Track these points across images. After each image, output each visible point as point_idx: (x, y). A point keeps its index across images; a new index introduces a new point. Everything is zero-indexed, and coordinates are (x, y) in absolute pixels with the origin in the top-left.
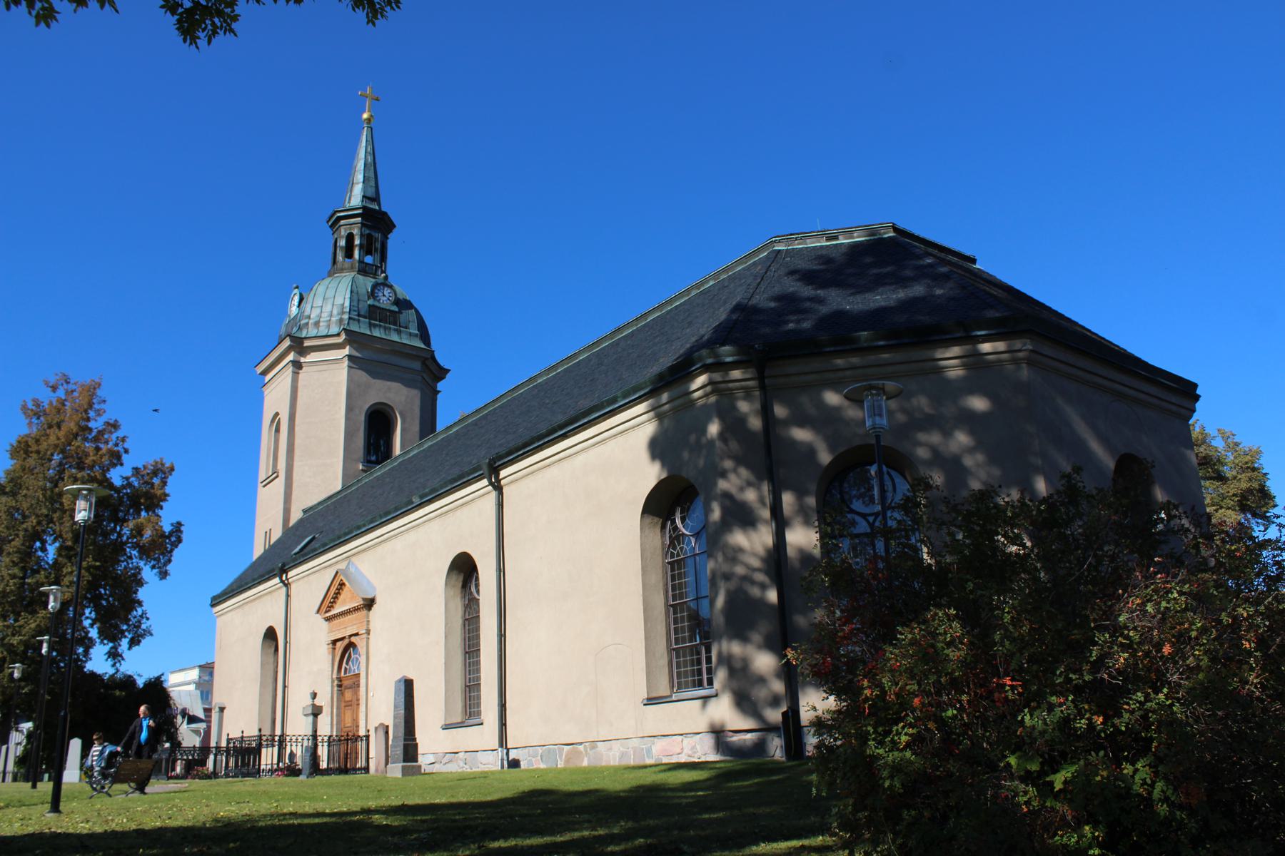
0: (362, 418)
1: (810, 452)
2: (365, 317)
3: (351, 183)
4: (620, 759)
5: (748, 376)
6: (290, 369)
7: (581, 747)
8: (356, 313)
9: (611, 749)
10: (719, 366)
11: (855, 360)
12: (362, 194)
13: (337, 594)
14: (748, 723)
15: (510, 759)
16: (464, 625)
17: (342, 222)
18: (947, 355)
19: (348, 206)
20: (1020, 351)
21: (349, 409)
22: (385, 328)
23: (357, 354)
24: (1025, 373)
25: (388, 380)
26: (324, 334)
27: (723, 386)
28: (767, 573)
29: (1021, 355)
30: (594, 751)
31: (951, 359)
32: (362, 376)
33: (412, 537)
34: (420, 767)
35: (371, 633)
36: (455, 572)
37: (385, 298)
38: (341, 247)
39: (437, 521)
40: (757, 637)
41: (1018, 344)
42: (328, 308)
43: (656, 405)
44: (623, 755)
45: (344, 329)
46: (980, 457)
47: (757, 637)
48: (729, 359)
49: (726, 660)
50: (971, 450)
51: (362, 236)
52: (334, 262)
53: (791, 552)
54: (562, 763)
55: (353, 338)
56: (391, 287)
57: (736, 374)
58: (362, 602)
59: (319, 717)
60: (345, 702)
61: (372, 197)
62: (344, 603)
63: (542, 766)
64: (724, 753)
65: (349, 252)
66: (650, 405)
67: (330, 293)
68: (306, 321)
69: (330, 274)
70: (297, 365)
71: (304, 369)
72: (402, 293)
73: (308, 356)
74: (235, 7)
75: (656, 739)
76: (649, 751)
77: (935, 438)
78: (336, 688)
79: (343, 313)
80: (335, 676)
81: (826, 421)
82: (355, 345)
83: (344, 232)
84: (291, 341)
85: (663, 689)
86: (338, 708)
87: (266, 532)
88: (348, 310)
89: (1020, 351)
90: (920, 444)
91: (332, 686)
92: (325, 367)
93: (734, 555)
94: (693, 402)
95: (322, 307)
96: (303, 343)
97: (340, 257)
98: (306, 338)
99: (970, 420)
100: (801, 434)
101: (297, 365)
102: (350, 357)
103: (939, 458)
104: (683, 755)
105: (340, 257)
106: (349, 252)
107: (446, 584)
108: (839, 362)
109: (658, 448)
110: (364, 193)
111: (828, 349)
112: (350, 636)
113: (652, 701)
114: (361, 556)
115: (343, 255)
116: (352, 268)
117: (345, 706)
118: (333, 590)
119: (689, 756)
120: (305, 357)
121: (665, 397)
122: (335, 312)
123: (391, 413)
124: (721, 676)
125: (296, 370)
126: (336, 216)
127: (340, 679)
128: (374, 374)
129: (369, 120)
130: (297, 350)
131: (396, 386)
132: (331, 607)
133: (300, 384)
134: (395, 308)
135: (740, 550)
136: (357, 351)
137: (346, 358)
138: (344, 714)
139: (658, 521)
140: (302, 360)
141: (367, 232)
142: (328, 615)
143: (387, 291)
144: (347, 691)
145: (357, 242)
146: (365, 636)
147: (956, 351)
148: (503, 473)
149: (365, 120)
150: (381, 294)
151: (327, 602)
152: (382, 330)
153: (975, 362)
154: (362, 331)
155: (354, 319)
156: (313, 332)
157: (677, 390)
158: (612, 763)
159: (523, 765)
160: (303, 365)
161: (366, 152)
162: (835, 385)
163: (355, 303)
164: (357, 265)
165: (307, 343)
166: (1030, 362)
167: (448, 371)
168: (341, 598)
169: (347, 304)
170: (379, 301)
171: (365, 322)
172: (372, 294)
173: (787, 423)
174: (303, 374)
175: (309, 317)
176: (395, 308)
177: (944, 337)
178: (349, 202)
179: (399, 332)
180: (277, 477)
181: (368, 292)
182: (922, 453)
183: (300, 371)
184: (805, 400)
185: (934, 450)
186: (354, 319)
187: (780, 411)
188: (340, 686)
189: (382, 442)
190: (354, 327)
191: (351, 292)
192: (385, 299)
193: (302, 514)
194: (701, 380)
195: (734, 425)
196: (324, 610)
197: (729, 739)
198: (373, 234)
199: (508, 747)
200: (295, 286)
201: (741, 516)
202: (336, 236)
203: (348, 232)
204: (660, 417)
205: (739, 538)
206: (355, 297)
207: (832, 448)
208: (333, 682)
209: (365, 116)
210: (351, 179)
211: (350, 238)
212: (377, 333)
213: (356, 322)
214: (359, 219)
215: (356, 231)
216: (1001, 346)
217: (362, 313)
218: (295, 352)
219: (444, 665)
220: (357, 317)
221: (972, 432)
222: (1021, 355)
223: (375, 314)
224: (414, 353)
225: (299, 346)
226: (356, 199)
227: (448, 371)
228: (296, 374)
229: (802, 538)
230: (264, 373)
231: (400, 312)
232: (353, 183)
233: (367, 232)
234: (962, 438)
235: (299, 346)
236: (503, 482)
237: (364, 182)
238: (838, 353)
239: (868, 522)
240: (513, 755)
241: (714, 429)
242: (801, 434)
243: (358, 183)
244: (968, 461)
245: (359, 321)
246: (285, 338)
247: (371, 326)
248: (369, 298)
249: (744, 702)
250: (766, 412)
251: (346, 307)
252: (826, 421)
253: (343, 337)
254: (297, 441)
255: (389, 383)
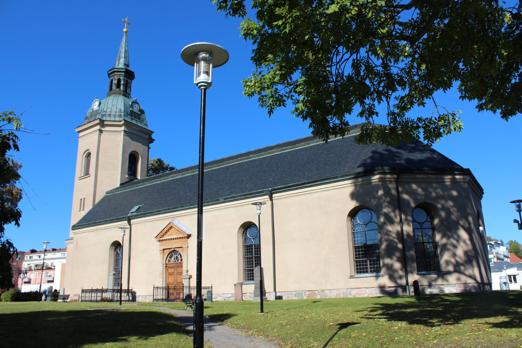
0: (128, 156)
1: (408, 202)
2: (129, 115)
3: (118, 57)
4: (336, 296)
5: (391, 177)
6: (98, 132)
7: (316, 292)
8: (126, 113)
9: (331, 292)
10: (384, 173)
11: (422, 176)
12: (124, 63)
13: (166, 233)
14: (392, 284)
15: (277, 296)
16: (243, 247)
17: (116, 73)
18: (447, 178)
19: (118, 67)
20: (466, 179)
21: (124, 152)
22: (136, 121)
23: (126, 130)
24: (466, 185)
25: (137, 142)
26: (109, 120)
27: (384, 179)
28: (397, 239)
29: (466, 180)
30: (323, 293)
31: (448, 179)
32: (128, 139)
33: (216, 213)
34: (267, 298)
35: (189, 247)
36: (242, 228)
37: (136, 108)
38: (115, 84)
39: (232, 208)
40: (395, 258)
41: (465, 177)
42: (114, 109)
43: (356, 182)
44: (337, 294)
45: (124, 119)
46: (455, 209)
47: (395, 258)
48: (388, 171)
49: (385, 265)
50: (452, 207)
51: (124, 80)
52: (111, 89)
53: (405, 233)
54: (306, 297)
55: (127, 124)
56: (138, 104)
57: (388, 176)
58: (187, 236)
59: (191, 279)
60: (169, 273)
61: (127, 65)
62: (172, 235)
63: (295, 298)
64: (383, 294)
65: (118, 85)
66: (353, 181)
67: (115, 103)
68: (105, 113)
69: (109, 95)
70: (101, 131)
71: (103, 133)
72: (142, 108)
73: (105, 128)
74: (438, 90)
75: (353, 289)
76: (350, 294)
77: (443, 202)
78: (165, 268)
79: (121, 112)
80: (164, 263)
81: (413, 193)
82: (126, 126)
83: (116, 78)
84: (100, 121)
85: (353, 274)
86: (166, 275)
87: (81, 199)
88: (123, 111)
89: (466, 179)
90: (439, 203)
91: (163, 267)
92: (112, 134)
93: (388, 233)
94: (371, 183)
95: (111, 108)
96: (104, 122)
97: (114, 87)
98: (105, 121)
99: (452, 198)
100: (405, 196)
101: (101, 131)
102: (125, 131)
103: (444, 208)
104: (366, 294)
105: (114, 87)
106: (118, 85)
107: (238, 232)
108: (418, 176)
109: (354, 196)
110: (125, 62)
111: (416, 172)
112: (175, 248)
113: (352, 277)
114: (181, 217)
115: (116, 87)
116: (120, 94)
117: (169, 275)
118: (165, 230)
119: (369, 295)
120: (104, 128)
121: (360, 180)
122: (117, 111)
123: (137, 154)
124: (383, 271)
125: (100, 133)
126: (113, 70)
127: (166, 264)
128: (133, 139)
129: (126, 32)
130: (101, 125)
131: (140, 144)
132: (163, 236)
133: (101, 139)
134: (139, 113)
135: (390, 231)
136: (127, 129)
137: (123, 131)
138: (168, 278)
139: (350, 218)
140: (103, 129)
141: (126, 79)
142: (161, 239)
143: (137, 105)
144: (169, 269)
145: (122, 82)
146: (187, 248)
147: (449, 177)
148: (274, 195)
149: (124, 32)
150: (134, 106)
151: (162, 234)
152: (135, 121)
153: (453, 181)
154: (129, 120)
155: (126, 116)
156: (108, 119)
157: (365, 178)
158: (332, 297)
159: (284, 298)
160: (103, 131)
161: (125, 46)
162: (415, 183)
163: (126, 109)
164: (122, 92)
165: (106, 123)
166: (468, 183)
167: (154, 140)
168: (169, 233)
169: (123, 109)
170: (134, 109)
171: (129, 117)
172: (132, 106)
173: (402, 192)
174: (103, 135)
175: (106, 112)
176: (139, 113)
177: (448, 172)
178: (118, 65)
179: (141, 123)
180: (90, 176)
181: (130, 105)
182: (439, 206)
183: (102, 134)
184: (407, 186)
185: (443, 206)
186: (126, 116)
187: (400, 189)
188: (166, 267)
189: (133, 167)
190: (126, 119)
191: (124, 104)
192: (136, 109)
193: (106, 194)
194: (377, 177)
195: (387, 192)
196: (159, 237)
197: (387, 289)
198: (128, 80)
199: (277, 291)
200: (96, 97)
201: (391, 221)
202: (112, 78)
203: (118, 78)
204: (356, 186)
205: (390, 228)
206: (126, 106)
207: (415, 202)
208: (163, 265)
209: (125, 30)
210: (118, 55)
211: (119, 81)
212: (134, 122)
213: (126, 117)
214: (123, 73)
215: (122, 78)
216: (461, 177)
217: (128, 113)
218: (100, 125)
219: (237, 262)
220: (126, 115)
221: (452, 201)
222: (466, 180)
223: (132, 114)
224: (147, 132)
225: (102, 123)
226: (121, 64)
227: (154, 140)
228: (100, 135)
229: (408, 229)
230: (79, 132)
231: (141, 115)
232: (120, 57)
233: (126, 79)
234: (450, 203)
235: (102, 123)
236: (273, 198)
237: (124, 58)
238: (419, 174)
239: (420, 225)
240: (278, 294)
241: (381, 192)
242: (405, 196)
243: (122, 58)
244: (452, 210)
245: (127, 116)
246: (98, 119)
247: (132, 119)
248: (130, 108)
249: (392, 277)
250: (397, 189)
251: (122, 110)
252: (413, 193)
253: (123, 122)
254: (100, 163)
255: (137, 143)
